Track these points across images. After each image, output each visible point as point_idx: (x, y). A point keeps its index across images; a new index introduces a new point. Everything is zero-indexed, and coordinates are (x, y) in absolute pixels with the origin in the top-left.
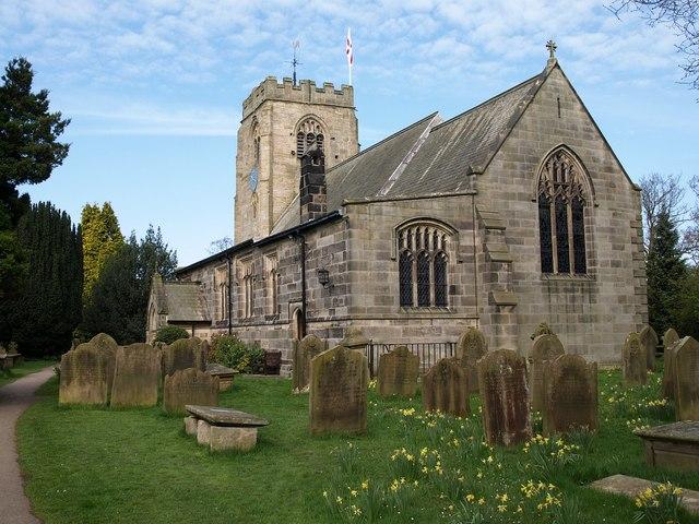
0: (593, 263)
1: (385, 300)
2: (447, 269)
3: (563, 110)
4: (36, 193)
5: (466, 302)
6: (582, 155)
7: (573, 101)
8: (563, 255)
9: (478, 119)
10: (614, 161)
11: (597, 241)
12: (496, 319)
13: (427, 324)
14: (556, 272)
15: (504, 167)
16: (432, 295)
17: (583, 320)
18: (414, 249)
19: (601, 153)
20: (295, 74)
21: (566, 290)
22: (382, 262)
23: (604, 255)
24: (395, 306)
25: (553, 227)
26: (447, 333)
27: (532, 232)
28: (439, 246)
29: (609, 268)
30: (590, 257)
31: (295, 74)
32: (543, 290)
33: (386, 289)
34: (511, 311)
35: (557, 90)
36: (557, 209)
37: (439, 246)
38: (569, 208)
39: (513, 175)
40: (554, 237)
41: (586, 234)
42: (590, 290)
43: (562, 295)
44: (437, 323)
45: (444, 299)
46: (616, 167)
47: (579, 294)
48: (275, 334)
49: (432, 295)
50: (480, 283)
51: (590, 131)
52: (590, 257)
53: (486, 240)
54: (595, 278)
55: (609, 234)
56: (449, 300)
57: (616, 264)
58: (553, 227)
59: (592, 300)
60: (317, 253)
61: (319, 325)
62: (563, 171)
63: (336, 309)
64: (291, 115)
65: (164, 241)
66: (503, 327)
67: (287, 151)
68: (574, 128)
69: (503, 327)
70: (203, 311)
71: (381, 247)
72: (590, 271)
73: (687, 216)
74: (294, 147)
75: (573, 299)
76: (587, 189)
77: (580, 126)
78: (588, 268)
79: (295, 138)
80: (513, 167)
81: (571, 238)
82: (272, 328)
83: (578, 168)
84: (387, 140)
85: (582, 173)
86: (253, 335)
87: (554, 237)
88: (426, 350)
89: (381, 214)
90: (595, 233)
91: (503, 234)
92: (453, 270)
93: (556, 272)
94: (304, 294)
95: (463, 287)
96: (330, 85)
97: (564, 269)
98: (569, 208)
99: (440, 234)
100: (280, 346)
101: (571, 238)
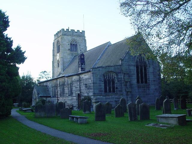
8: (142, 79)
13: (111, 97)
18: (107, 79)
21: (143, 87)
28: (113, 78)
33: (101, 88)
37: (113, 78)
38: (143, 67)
42: (148, 88)
48: (72, 99)
59: (149, 90)
71: (100, 78)
79: (69, 45)
92: (116, 83)
93: (108, 92)
98: (143, 67)
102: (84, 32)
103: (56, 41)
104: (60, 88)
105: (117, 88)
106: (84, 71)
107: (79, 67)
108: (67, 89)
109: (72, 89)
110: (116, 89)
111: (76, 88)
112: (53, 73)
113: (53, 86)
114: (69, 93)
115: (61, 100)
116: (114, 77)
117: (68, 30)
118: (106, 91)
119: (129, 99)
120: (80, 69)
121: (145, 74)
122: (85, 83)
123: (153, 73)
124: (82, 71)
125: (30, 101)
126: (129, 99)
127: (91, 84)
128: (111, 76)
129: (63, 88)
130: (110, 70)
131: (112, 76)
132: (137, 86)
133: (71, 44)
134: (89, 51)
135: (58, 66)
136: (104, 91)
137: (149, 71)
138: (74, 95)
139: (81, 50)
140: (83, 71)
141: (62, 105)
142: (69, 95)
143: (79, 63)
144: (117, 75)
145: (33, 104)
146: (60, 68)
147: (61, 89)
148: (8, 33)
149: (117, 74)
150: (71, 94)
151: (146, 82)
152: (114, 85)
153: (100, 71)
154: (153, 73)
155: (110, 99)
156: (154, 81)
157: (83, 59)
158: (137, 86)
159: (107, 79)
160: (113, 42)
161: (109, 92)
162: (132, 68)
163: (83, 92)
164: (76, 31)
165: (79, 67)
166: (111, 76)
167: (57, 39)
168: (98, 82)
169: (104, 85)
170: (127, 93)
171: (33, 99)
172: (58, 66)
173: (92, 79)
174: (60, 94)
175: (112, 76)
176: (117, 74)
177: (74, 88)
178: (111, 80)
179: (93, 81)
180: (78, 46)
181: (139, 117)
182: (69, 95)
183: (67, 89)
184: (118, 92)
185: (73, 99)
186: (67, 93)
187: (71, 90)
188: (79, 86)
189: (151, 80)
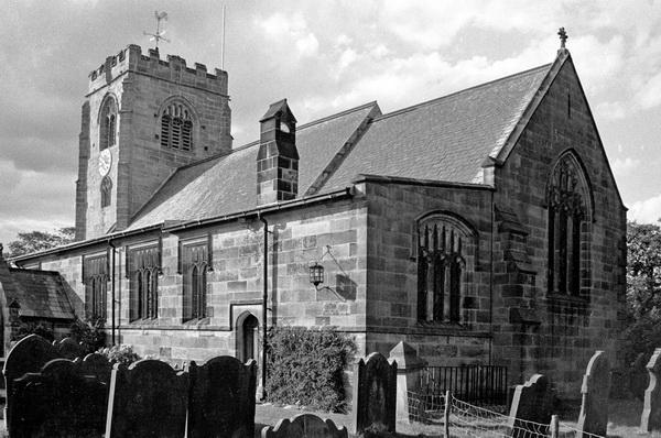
0: (588, 283)
1: (400, 309)
2: (462, 279)
5: (482, 318)
10: (609, 175)
12: (522, 339)
13: (443, 341)
17: (578, 344)
18: (431, 249)
21: (566, 311)
22: (402, 261)
23: (597, 276)
24: (413, 320)
26: (463, 354)
27: (541, 243)
28: (456, 250)
29: (600, 290)
30: (584, 277)
32: (549, 309)
34: (534, 331)
44: (453, 341)
45: (458, 313)
46: (610, 181)
50: (498, 295)
51: (593, 138)
52: (584, 277)
53: (510, 246)
54: (588, 299)
55: (601, 254)
57: (605, 286)
60: (292, 244)
66: (527, 348)
69: (527, 348)
71: (399, 241)
72: (584, 291)
77: (585, 130)
78: (582, 288)
83: (581, 176)
85: (584, 183)
86: (156, 340)
88: (443, 374)
90: (592, 252)
91: (524, 241)
92: (469, 278)
95: (479, 299)
96: (201, 67)
99: (449, 228)
105: (469, 302)
106: (290, 205)
107: (260, 178)
111: (234, 285)
113: (136, 266)
118: (422, 315)
119: (528, 359)
123: (604, 250)
124: (279, 198)
126: (528, 359)
130: (446, 204)
132: (548, 302)
133: (166, 119)
137: (590, 239)
138: (220, 319)
139: (206, 148)
142: (184, 321)
144: (476, 237)
147: (137, 291)
149: (476, 233)
150: (196, 308)
154: (604, 250)
155: (439, 354)
156: (605, 286)
157: (291, 137)
158: (548, 302)
159: (431, 249)
162: (534, 212)
164: (190, 65)
165: (260, 178)
167: (104, 91)
168: (390, 260)
170: (523, 329)
172: (105, 202)
173: (362, 241)
176: (476, 233)
178: (446, 256)
182: (184, 321)
184: (475, 322)
185: (210, 341)
186: (173, 312)
189: (594, 279)
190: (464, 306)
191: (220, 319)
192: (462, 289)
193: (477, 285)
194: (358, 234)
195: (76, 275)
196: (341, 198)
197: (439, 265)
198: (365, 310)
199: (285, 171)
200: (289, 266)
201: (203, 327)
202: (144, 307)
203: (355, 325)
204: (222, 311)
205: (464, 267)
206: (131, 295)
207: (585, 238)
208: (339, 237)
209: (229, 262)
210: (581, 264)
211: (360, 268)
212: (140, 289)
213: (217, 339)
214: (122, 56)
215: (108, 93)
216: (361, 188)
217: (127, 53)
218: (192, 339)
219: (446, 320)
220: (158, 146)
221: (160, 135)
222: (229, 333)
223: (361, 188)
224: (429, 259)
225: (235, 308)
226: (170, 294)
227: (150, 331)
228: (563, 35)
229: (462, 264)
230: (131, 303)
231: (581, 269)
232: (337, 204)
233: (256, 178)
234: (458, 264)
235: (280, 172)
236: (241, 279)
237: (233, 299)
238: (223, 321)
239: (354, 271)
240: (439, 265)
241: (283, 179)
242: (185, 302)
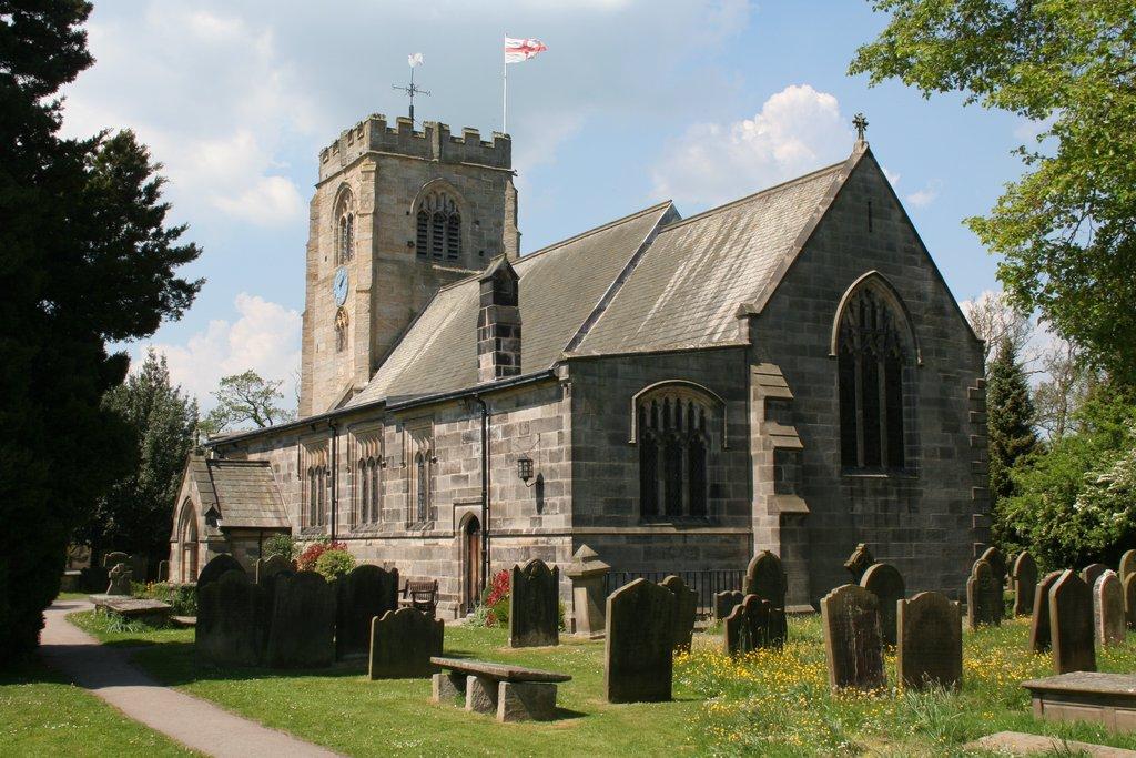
3: (875, 220)
4: (138, 352)
6: (903, 290)
7: (891, 207)
8: (872, 439)
9: (742, 224)
11: (921, 419)
14: (861, 465)
15: (791, 305)
16: (685, 498)
17: (899, 536)
18: (661, 429)
19: (929, 287)
20: (412, 109)
21: (876, 492)
25: (858, 396)
28: (697, 424)
31: (412, 109)
33: (621, 489)
35: (867, 191)
36: (864, 368)
37: (697, 424)
38: (881, 367)
39: (804, 319)
40: (859, 412)
41: (905, 408)
42: (910, 498)
43: (870, 500)
47: (893, 498)
48: (426, 553)
49: (685, 498)
56: (708, 505)
58: (858, 396)
59: (913, 508)
61: (513, 541)
62: (874, 312)
63: (544, 517)
64: (407, 181)
65: (173, 383)
67: (401, 241)
68: (891, 248)
70: (276, 511)
73: (1039, 365)
74: (413, 235)
75: (886, 505)
76: (907, 339)
79: (414, 220)
80: (804, 306)
81: (883, 412)
82: (421, 543)
84: (586, 234)
87: (859, 412)
89: (615, 376)
92: (715, 460)
93: (861, 465)
94: (486, 493)
97: (872, 463)
98: (881, 367)
100: (435, 572)
101: (883, 412)
102: (504, 144)
103: (331, 189)
104: (353, 480)
108: (397, 488)
109: (432, 482)
110: (908, 443)
111: (457, 479)
112: (307, 384)
114: (409, 513)
115: (361, 553)
116: (702, 420)
117: (406, 125)
120: (488, 361)
121: (889, 411)
122: (517, 453)
124: (498, 373)
125: (155, 568)
127: (555, 456)
128: (684, 414)
129: (375, 479)
131: (691, 412)
134: (533, 255)
135: (341, 344)
136: (636, 505)
138: (445, 523)
140: (507, 373)
141: (376, 584)
143: (481, 322)
145: (179, 572)
146: (351, 352)
147: (360, 486)
148: (79, 141)
150: (619, 471)
151: (896, 462)
152: (702, 470)
153: (619, 381)
155: (673, 557)
156: (947, 454)
160: (80, 72)
161: (669, 512)
163: (502, 510)
166: (684, 414)
167: (338, 181)
169: (637, 465)
171: (175, 547)
172: (341, 344)
173: (567, 429)
174: (353, 517)
175: (691, 412)
177: (443, 484)
179: (573, 442)
180: (466, 226)
181: (892, 664)
182: (408, 526)
183: (397, 488)
184: (725, 515)
185: (435, 550)
186: (397, 514)
187: (426, 494)
188: (480, 469)
190: (712, 496)
191: (445, 523)
192: (708, 476)
193: (726, 468)
194: (564, 421)
195: (290, 465)
196: (545, 380)
197: (673, 452)
198: (570, 508)
199: (505, 341)
200: (507, 456)
201: (428, 533)
202: (371, 506)
203: (564, 527)
204: (446, 512)
205: (709, 447)
206: (353, 493)
207: (909, 390)
208: (544, 430)
209: (452, 453)
210: (905, 426)
211: (567, 460)
212: (365, 483)
213: (441, 548)
214: (360, 128)
215: (343, 184)
216: (563, 373)
217: (367, 129)
218: (417, 548)
219: (685, 515)
220: (412, 256)
221: (415, 241)
222: (452, 541)
223: (563, 373)
224: (659, 441)
225: (457, 508)
226: (394, 492)
227: (373, 541)
228: (861, 124)
229: (706, 443)
230: (354, 504)
231: (905, 432)
232: (545, 385)
233: (476, 349)
234: (702, 443)
235: (498, 343)
236: (463, 473)
237: (456, 498)
238: (446, 525)
239: (561, 463)
240: (673, 452)
241: (502, 351)
242: (409, 502)
